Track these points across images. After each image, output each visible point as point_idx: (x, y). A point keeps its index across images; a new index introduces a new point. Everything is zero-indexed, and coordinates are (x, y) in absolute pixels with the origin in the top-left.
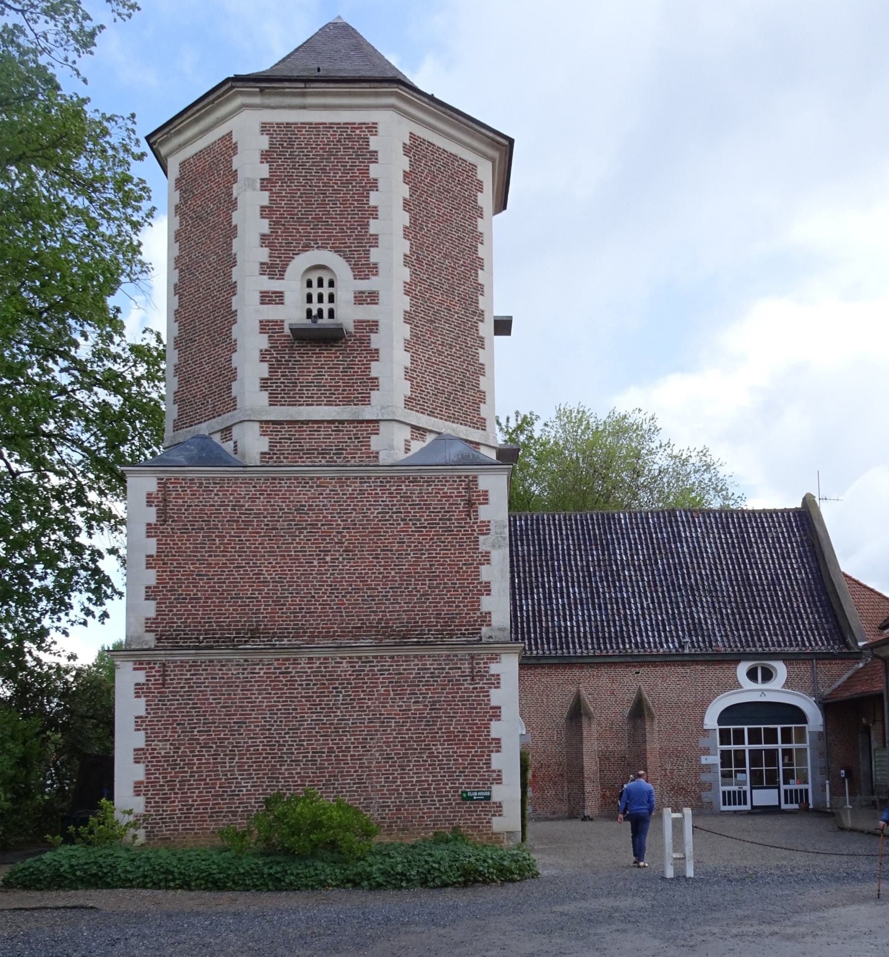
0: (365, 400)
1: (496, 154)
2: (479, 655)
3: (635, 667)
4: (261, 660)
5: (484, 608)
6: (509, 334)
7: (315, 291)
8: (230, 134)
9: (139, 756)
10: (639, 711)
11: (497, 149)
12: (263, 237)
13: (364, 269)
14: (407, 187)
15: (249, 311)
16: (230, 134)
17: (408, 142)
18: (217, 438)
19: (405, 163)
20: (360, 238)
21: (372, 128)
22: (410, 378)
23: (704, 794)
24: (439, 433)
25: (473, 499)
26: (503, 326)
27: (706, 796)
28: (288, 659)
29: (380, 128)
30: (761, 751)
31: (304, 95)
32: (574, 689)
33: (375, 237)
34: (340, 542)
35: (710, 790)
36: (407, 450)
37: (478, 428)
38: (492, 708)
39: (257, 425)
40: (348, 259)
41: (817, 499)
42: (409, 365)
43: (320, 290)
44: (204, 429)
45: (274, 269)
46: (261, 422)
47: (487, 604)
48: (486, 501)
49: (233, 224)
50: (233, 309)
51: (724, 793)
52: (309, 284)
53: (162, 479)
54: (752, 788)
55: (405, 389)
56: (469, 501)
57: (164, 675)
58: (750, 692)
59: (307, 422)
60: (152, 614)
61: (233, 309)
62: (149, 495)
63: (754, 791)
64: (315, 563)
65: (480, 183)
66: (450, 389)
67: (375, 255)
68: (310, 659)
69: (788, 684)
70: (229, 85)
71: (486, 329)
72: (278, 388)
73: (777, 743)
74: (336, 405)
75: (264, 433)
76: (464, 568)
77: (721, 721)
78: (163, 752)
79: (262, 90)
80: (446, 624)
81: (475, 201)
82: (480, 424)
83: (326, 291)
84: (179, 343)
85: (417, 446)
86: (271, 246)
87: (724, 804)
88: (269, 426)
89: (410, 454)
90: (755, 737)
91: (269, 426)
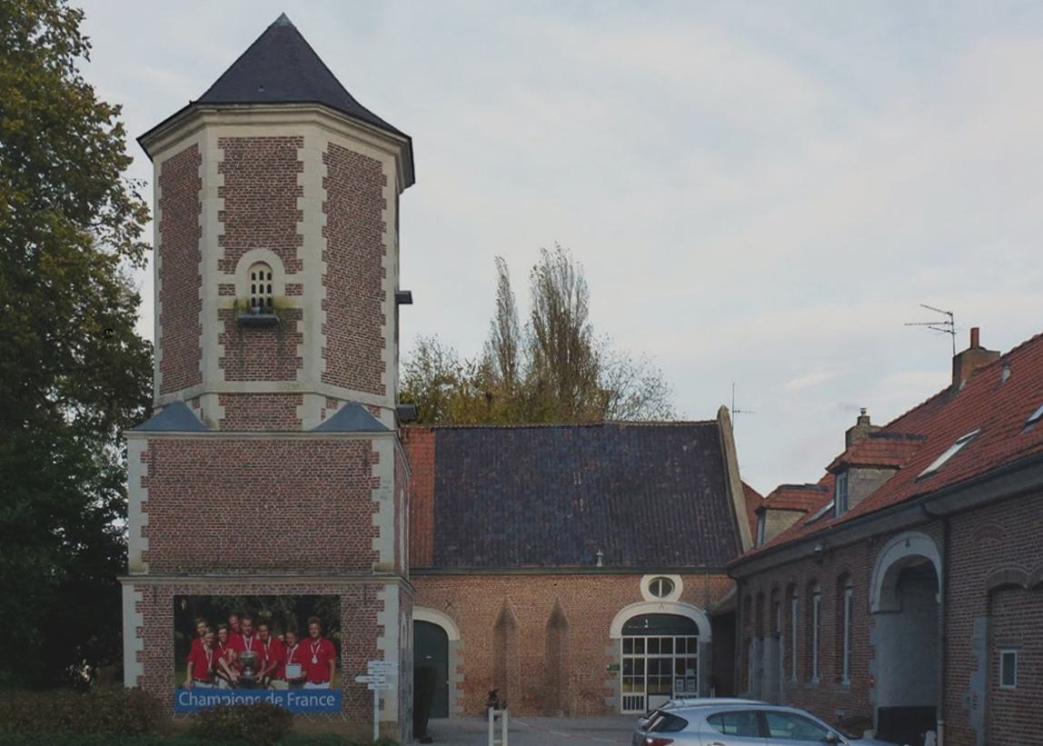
0: (293, 376)
1: (397, 150)
2: (369, 584)
3: (554, 579)
4: (221, 586)
5: (375, 548)
6: (411, 302)
7: (258, 283)
8: (196, 145)
9: (140, 656)
10: (557, 621)
11: (398, 145)
12: (221, 237)
13: (293, 265)
14: (325, 191)
15: (212, 301)
16: (196, 145)
17: (327, 152)
18: (189, 404)
19: (323, 170)
20: (289, 238)
21: (299, 141)
22: (326, 357)
23: (607, 699)
24: (348, 401)
25: (369, 459)
26: (405, 298)
27: (609, 701)
28: (238, 586)
29: (306, 141)
30: (657, 660)
31: (249, 114)
32: (502, 599)
33: (301, 237)
34: (274, 494)
35: (612, 695)
36: (323, 417)
37: (379, 394)
38: (378, 626)
39: (217, 396)
40: (281, 256)
41: (730, 413)
42: (325, 346)
43: (262, 282)
44: (180, 395)
45: (228, 265)
46: (219, 394)
47: (377, 544)
48: (377, 462)
49: (200, 225)
50: (200, 298)
51: (625, 698)
52: (254, 277)
53: (151, 440)
54: (649, 694)
55: (322, 365)
56: (366, 461)
57: (155, 596)
58: (651, 604)
59: (252, 394)
60: (146, 548)
61: (200, 298)
62: (143, 454)
63: (650, 697)
64: (257, 509)
65: (385, 178)
66: (357, 362)
67: (301, 253)
68: (254, 585)
69: (684, 598)
70: (193, 108)
71: (387, 307)
72: (235, 369)
73: (671, 652)
74: (272, 380)
75: (222, 404)
76: (361, 515)
77: (625, 630)
78: (155, 654)
79: (219, 110)
80: (348, 560)
81: (380, 195)
82: (381, 390)
83: (265, 283)
84: (162, 342)
85: (330, 413)
86: (226, 244)
87: (625, 708)
88: (225, 398)
89: (325, 420)
90: (653, 646)
91: (225, 398)
